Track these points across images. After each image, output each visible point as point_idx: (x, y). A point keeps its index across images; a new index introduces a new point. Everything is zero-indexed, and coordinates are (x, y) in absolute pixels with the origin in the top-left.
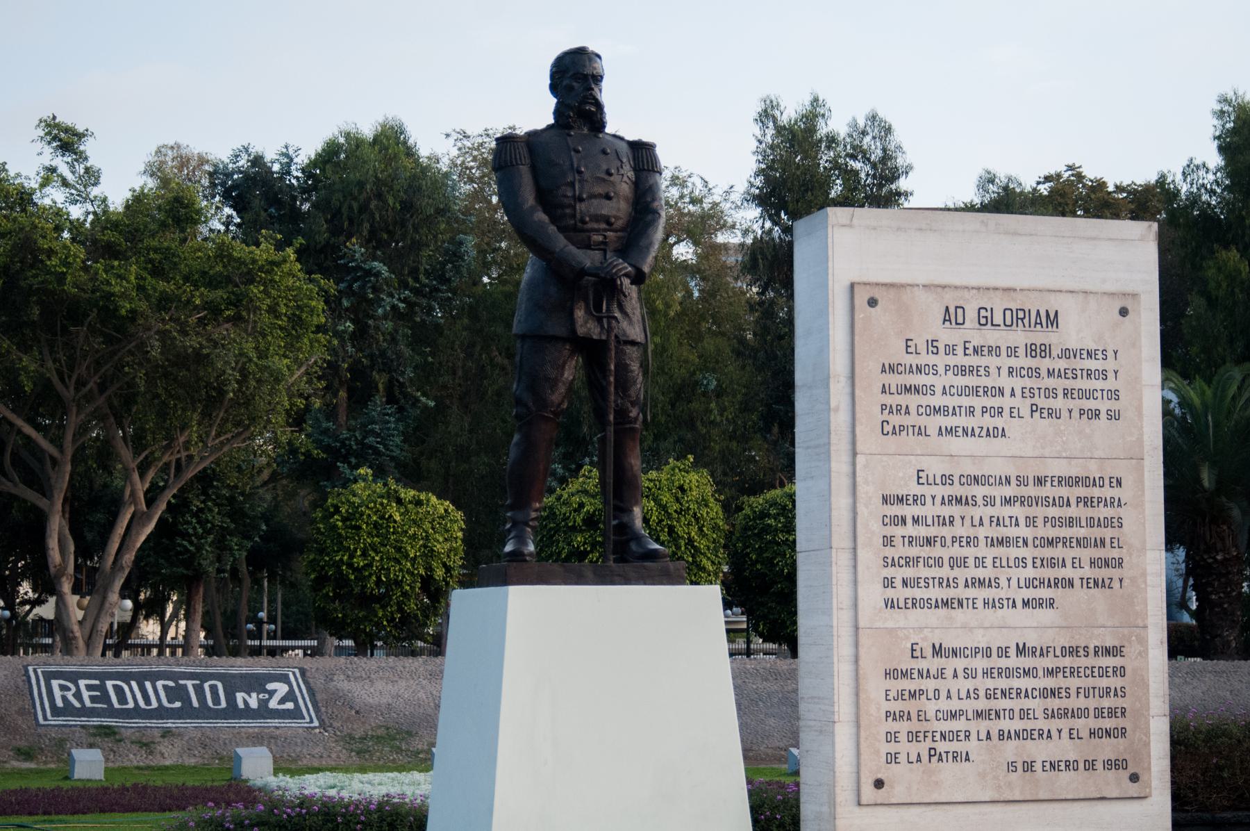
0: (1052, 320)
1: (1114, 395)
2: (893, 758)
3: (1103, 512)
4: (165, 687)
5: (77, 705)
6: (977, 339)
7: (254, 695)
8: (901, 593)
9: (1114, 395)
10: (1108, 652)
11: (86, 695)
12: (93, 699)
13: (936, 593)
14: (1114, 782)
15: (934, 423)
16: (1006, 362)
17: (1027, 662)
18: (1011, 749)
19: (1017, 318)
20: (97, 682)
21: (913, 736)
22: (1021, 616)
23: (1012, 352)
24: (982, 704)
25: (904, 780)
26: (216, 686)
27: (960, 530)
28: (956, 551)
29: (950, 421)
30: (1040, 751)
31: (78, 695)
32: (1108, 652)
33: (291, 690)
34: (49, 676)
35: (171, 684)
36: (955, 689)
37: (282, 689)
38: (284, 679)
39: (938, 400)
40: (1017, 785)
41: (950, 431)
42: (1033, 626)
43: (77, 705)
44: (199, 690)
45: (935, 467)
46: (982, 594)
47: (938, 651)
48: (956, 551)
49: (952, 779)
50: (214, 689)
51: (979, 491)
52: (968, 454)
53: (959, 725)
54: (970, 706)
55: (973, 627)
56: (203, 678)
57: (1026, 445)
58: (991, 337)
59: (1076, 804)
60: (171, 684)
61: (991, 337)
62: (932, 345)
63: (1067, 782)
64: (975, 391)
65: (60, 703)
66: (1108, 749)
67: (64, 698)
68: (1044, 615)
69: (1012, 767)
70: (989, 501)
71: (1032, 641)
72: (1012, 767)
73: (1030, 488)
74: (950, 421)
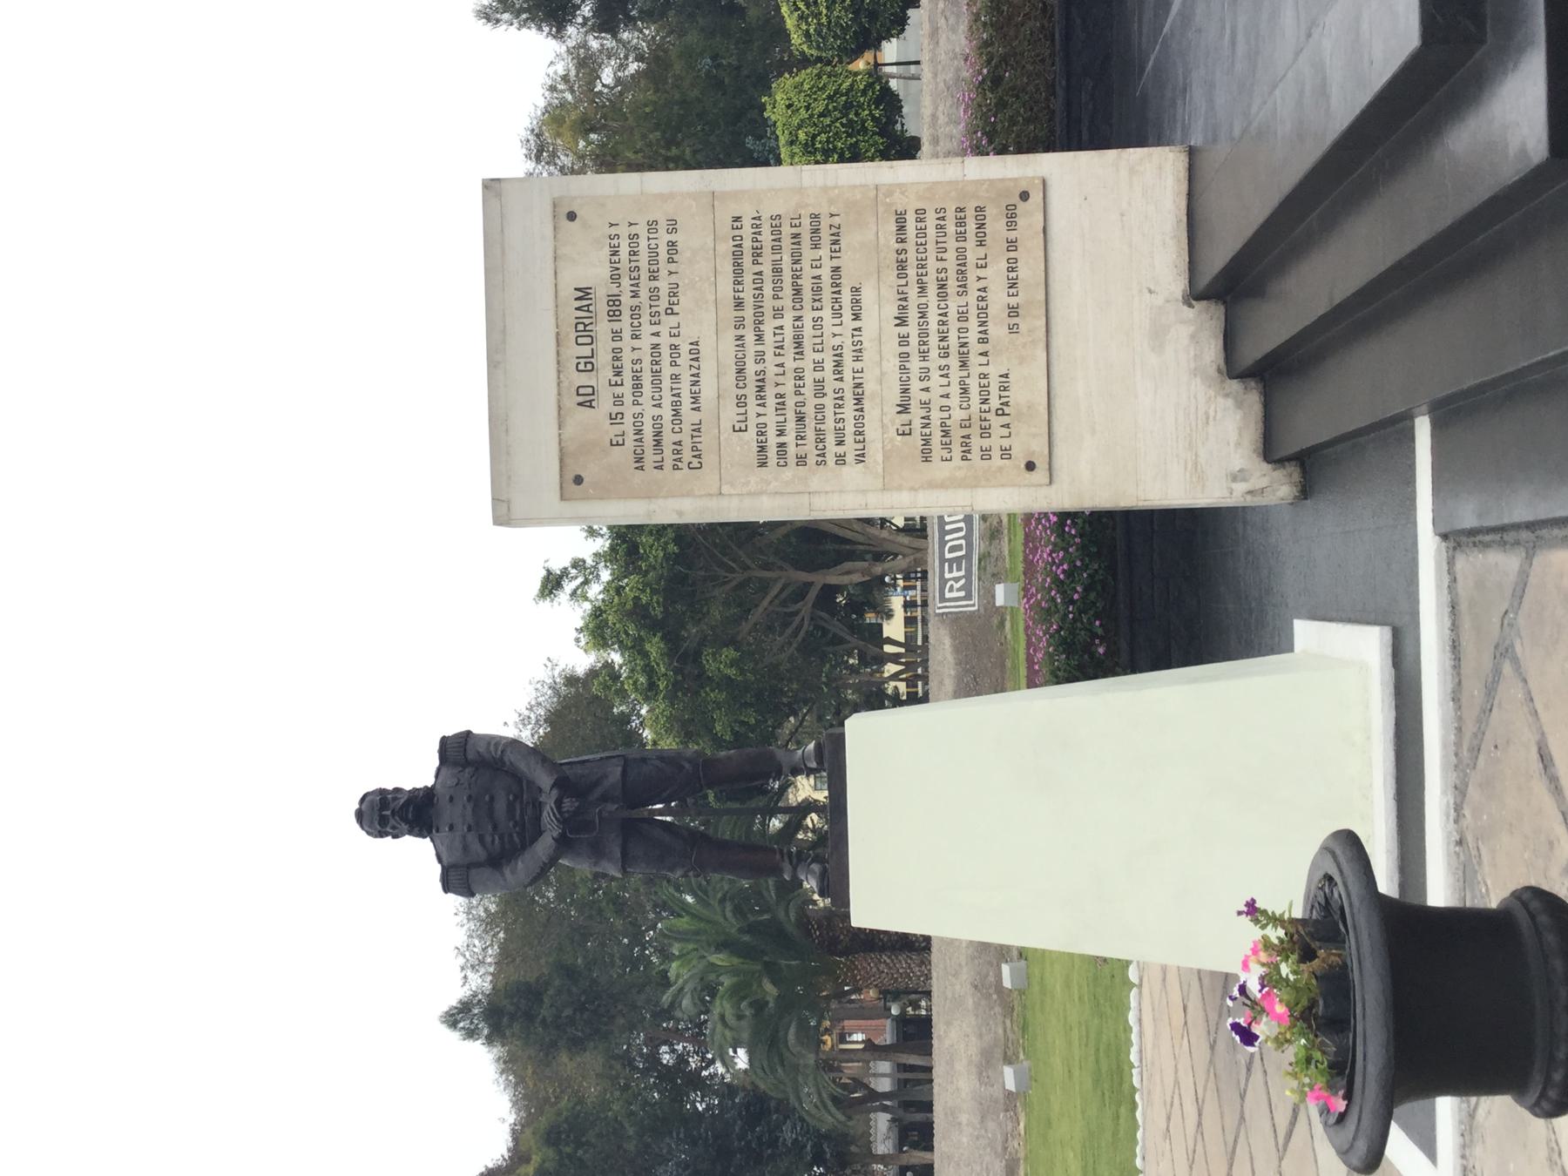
0: (584, 293)
1: (652, 225)
2: (1006, 453)
3: (766, 237)
9: (652, 225)
11: (955, 574)
12: (959, 569)
13: (849, 412)
14: (1030, 217)
15: (689, 416)
16: (627, 343)
17: (913, 315)
18: (997, 331)
19: (584, 330)
21: (985, 432)
22: (869, 322)
23: (617, 335)
24: (954, 361)
28: (808, 391)
30: (998, 299)
31: (957, 580)
34: (943, 599)
36: (939, 388)
39: (667, 412)
40: (1032, 323)
45: (730, 413)
46: (849, 364)
47: (904, 409)
48: (808, 391)
49: (1027, 391)
50: (960, 529)
51: (751, 368)
53: (974, 385)
54: (955, 374)
55: (881, 372)
57: (703, 320)
58: (604, 358)
61: (604, 358)
62: (615, 418)
63: (1029, 271)
65: (962, 594)
66: (996, 226)
68: (867, 296)
69: (1014, 329)
70: (760, 357)
73: (747, 315)
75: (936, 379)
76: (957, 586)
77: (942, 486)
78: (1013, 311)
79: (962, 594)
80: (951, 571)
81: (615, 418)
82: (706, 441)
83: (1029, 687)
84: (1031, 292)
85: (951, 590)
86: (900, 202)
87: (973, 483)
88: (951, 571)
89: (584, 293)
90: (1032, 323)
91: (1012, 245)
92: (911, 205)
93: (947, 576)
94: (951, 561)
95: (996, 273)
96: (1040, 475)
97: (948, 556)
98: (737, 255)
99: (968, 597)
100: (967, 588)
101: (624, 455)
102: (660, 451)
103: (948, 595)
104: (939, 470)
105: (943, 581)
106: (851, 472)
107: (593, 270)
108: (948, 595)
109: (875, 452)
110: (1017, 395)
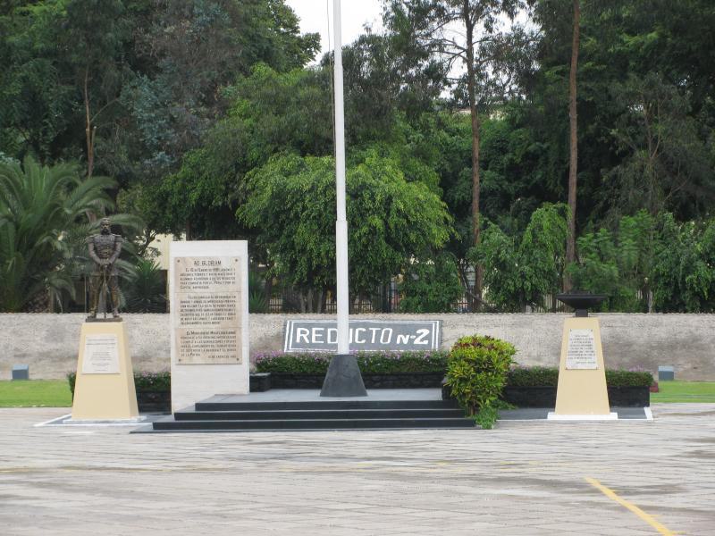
0: (220, 263)
1: (234, 278)
2: (183, 355)
3: (231, 304)
4: (360, 332)
5: (307, 341)
6: (202, 268)
7: (408, 336)
8: (185, 321)
9: (234, 278)
10: (232, 333)
11: (314, 336)
12: (317, 339)
13: (192, 321)
14: (234, 360)
15: (192, 286)
16: (209, 272)
17: (213, 335)
18: (210, 354)
19: (212, 263)
20: (322, 329)
21: (188, 351)
22: (212, 326)
23: (210, 270)
24: (203, 344)
25: (185, 360)
26: (389, 331)
27: (198, 308)
28: (197, 312)
29: (195, 285)
30: (217, 354)
31: (310, 337)
32: (232, 333)
33: (430, 334)
34: (297, 326)
35: (364, 330)
36: (197, 341)
37: (426, 332)
38: (429, 327)
39: (193, 281)
40: (210, 361)
41: (196, 287)
42: (214, 328)
43: (307, 341)
44: (378, 333)
45: (192, 295)
46: (202, 321)
47: (193, 333)
48: (197, 312)
49: (196, 359)
50: (387, 332)
51: (203, 300)
52: (200, 292)
53: (198, 348)
54: (200, 344)
55: (199, 328)
56: (382, 326)
57: (214, 289)
58: (205, 267)
59: (213, 366)
60: (364, 330)
61: (205, 267)
62: (192, 270)
63: (222, 360)
64: (200, 279)
65: (298, 341)
66: (232, 353)
67: (302, 338)
68: (217, 325)
69: (209, 357)
70: (205, 302)
71: (214, 330)
72: (209, 357)
73: (214, 299)
74: (195, 285)
75: (199, 340)
76: (305, 336)
77: (176, 342)
78: (213, 357)
79: (298, 341)
80: (317, 332)
81: (192, 270)
82: (187, 290)
83: (251, 378)
84: (216, 361)
85: (303, 332)
86: (238, 332)
87: (177, 348)
88: (317, 332)
89: (220, 263)
90: (210, 361)
91: (227, 357)
92: (237, 335)
93: (314, 329)
94: (325, 333)
95: (221, 353)
96: (178, 362)
97: (329, 330)
98: (227, 297)
99: (295, 345)
100: (303, 344)
101: (184, 271)
102: (184, 281)
103: (299, 330)
104: (179, 340)
105: (309, 326)
106: (179, 321)
107: (224, 265)
108: (299, 330)
109: (184, 326)
110: (195, 357)
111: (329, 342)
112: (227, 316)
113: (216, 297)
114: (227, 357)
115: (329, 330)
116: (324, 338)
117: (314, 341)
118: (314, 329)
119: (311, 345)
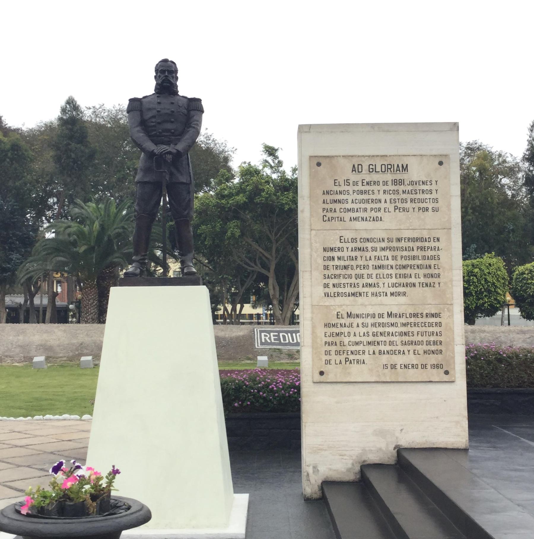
0: (405, 168)
1: (436, 200)
2: (328, 362)
3: (430, 253)
5: (269, 341)
6: (368, 178)
8: (332, 290)
9: (436, 200)
11: (272, 338)
12: (275, 340)
13: (348, 290)
14: (437, 375)
15: (347, 216)
16: (382, 188)
17: (393, 320)
18: (385, 359)
19: (388, 168)
21: (338, 353)
22: (390, 300)
23: (385, 183)
24: (371, 339)
25: (334, 372)
27: (360, 262)
28: (358, 271)
30: (399, 360)
31: (270, 338)
34: (261, 332)
36: (358, 332)
39: (349, 206)
41: (355, 219)
43: (269, 341)
45: (348, 235)
46: (371, 290)
47: (349, 315)
48: (358, 271)
49: (357, 372)
51: (369, 245)
54: (365, 339)
57: (392, 223)
58: (375, 177)
61: (375, 177)
62: (347, 182)
65: (263, 341)
66: (433, 359)
67: (265, 339)
69: (385, 366)
70: (374, 249)
73: (393, 244)
75: (363, 330)
77: (313, 332)
78: (394, 367)
79: (263, 341)
82: (336, 224)
85: (265, 336)
88: (274, 336)
89: (405, 168)
91: (424, 366)
94: (279, 336)
95: (411, 359)
96: (318, 378)
98: (421, 239)
100: (266, 343)
101: (330, 185)
103: (263, 334)
104: (321, 331)
106: (320, 290)
107: (416, 173)
108: (263, 334)
109: (329, 302)
110: (355, 367)
111: (282, 341)
112: (422, 280)
113: (399, 240)
114: (424, 366)
115: (281, 334)
116: (279, 339)
117: (273, 341)
118: (272, 334)
119: (271, 344)
